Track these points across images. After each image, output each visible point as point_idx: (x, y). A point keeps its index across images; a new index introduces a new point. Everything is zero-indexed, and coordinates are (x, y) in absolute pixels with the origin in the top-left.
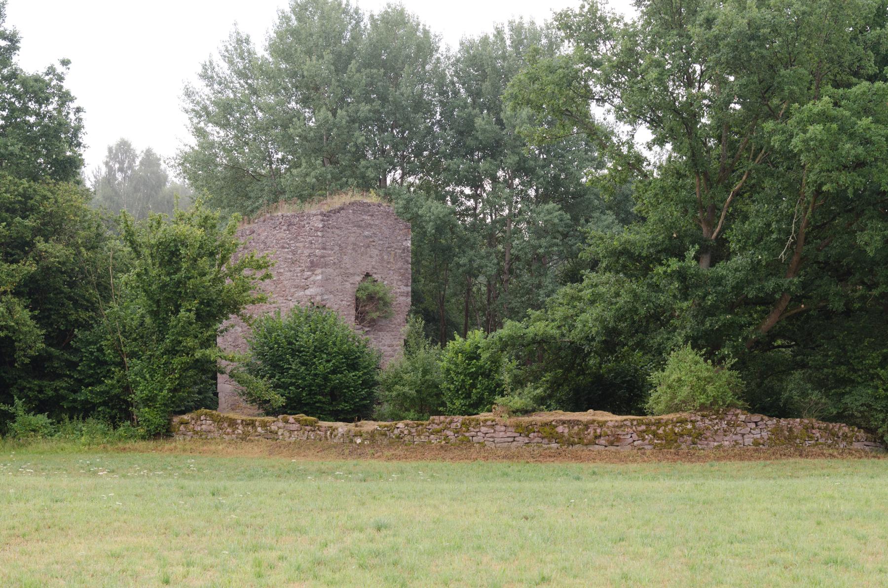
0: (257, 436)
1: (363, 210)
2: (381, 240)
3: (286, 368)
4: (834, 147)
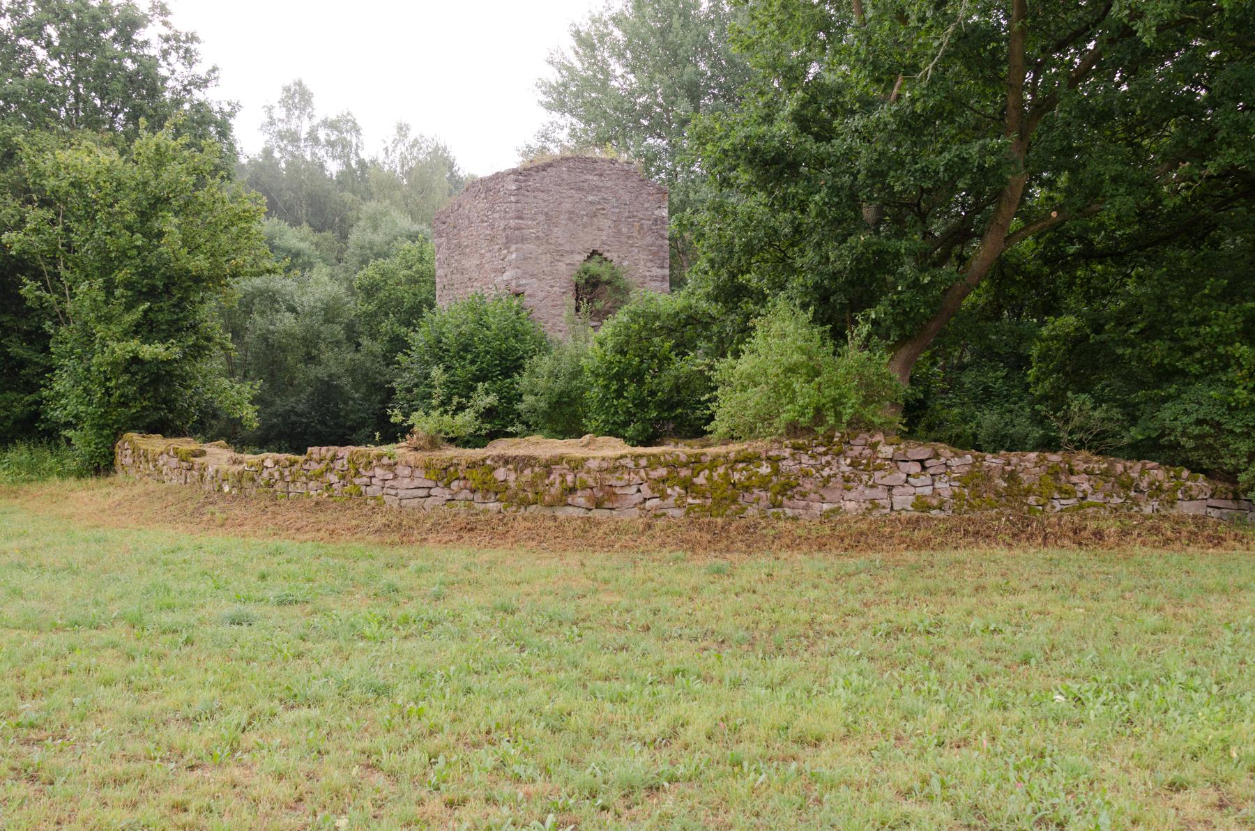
1: (585, 168)
2: (617, 207)
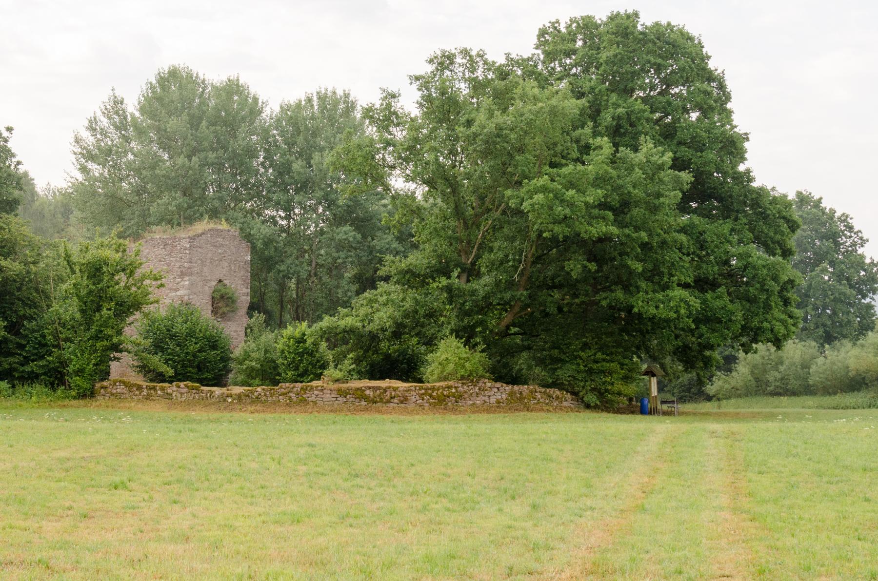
4: (551, 208)
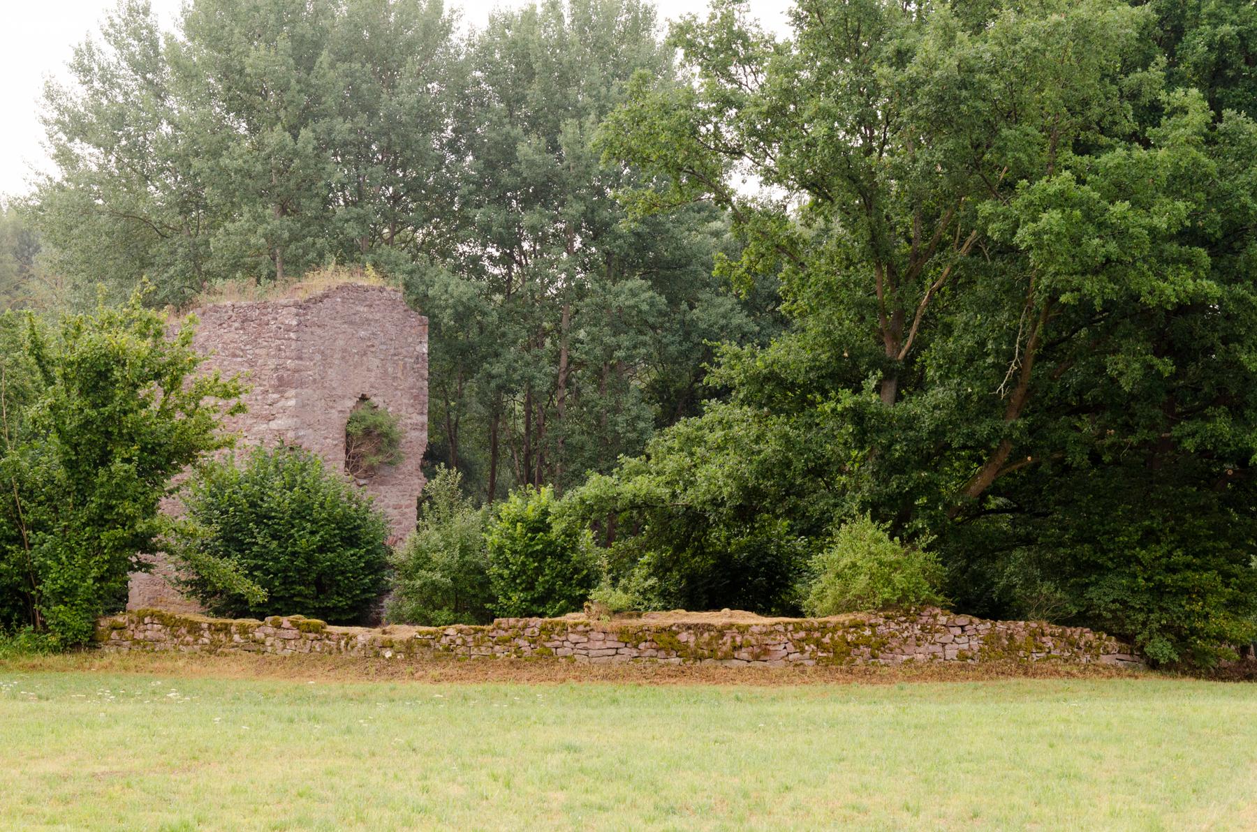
0: (233, 647)
3: (248, 543)
4: (1076, 241)
